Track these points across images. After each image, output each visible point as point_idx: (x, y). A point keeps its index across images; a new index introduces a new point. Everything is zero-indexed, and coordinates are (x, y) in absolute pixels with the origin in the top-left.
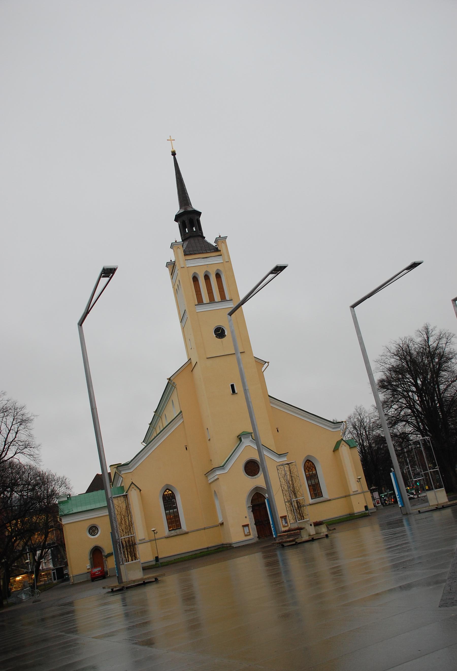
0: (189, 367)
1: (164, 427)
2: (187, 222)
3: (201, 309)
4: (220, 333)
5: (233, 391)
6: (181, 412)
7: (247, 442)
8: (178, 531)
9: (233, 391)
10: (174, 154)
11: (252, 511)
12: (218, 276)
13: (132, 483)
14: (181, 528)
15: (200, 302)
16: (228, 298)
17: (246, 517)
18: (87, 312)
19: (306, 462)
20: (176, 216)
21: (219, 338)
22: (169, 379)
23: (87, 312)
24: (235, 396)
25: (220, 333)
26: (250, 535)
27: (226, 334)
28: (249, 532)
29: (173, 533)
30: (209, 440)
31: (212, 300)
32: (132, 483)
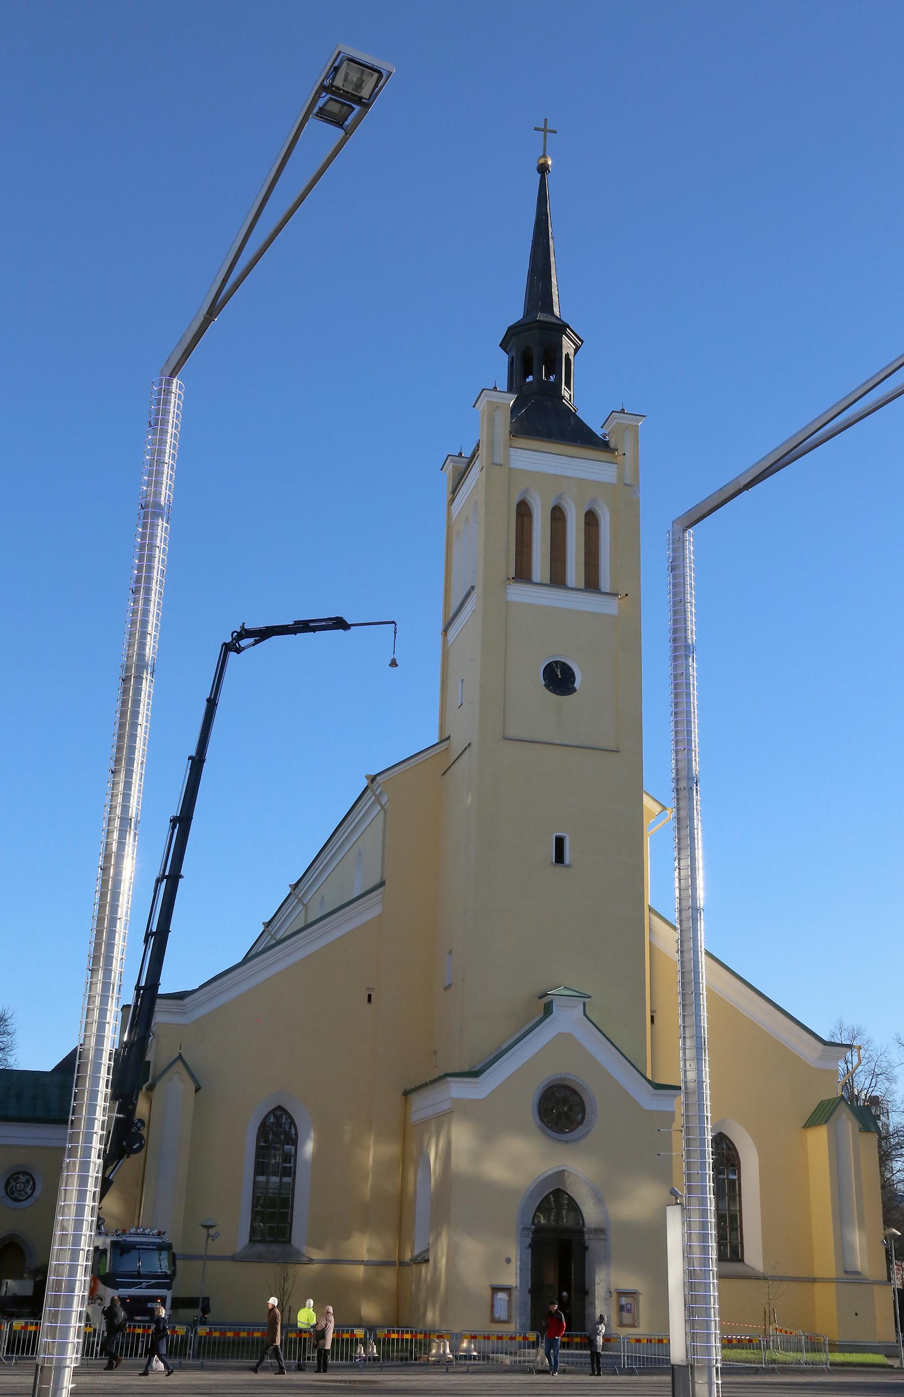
0: (440, 759)
1: (310, 921)
2: (536, 352)
3: (519, 593)
4: (559, 679)
5: (560, 857)
6: (382, 884)
7: (567, 1019)
8: (276, 1248)
9: (560, 857)
10: (543, 169)
11: (531, 1246)
12: (591, 520)
13: (180, 1057)
14: (289, 1241)
15: (523, 574)
16: (605, 583)
17: (508, 1261)
18: (213, 312)
19: (273, 1112)
20: (510, 328)
21: (554, 692)
22: (373, 779)
23: (213, 312)
24: (559, 869)
25: (559, 679)
26: (507, 1322)
27: (577, 685)
28: (510, 1316)
29: (261, 1248)
30: (447, 988)
31: (557, 579)
32: (180, 1057)
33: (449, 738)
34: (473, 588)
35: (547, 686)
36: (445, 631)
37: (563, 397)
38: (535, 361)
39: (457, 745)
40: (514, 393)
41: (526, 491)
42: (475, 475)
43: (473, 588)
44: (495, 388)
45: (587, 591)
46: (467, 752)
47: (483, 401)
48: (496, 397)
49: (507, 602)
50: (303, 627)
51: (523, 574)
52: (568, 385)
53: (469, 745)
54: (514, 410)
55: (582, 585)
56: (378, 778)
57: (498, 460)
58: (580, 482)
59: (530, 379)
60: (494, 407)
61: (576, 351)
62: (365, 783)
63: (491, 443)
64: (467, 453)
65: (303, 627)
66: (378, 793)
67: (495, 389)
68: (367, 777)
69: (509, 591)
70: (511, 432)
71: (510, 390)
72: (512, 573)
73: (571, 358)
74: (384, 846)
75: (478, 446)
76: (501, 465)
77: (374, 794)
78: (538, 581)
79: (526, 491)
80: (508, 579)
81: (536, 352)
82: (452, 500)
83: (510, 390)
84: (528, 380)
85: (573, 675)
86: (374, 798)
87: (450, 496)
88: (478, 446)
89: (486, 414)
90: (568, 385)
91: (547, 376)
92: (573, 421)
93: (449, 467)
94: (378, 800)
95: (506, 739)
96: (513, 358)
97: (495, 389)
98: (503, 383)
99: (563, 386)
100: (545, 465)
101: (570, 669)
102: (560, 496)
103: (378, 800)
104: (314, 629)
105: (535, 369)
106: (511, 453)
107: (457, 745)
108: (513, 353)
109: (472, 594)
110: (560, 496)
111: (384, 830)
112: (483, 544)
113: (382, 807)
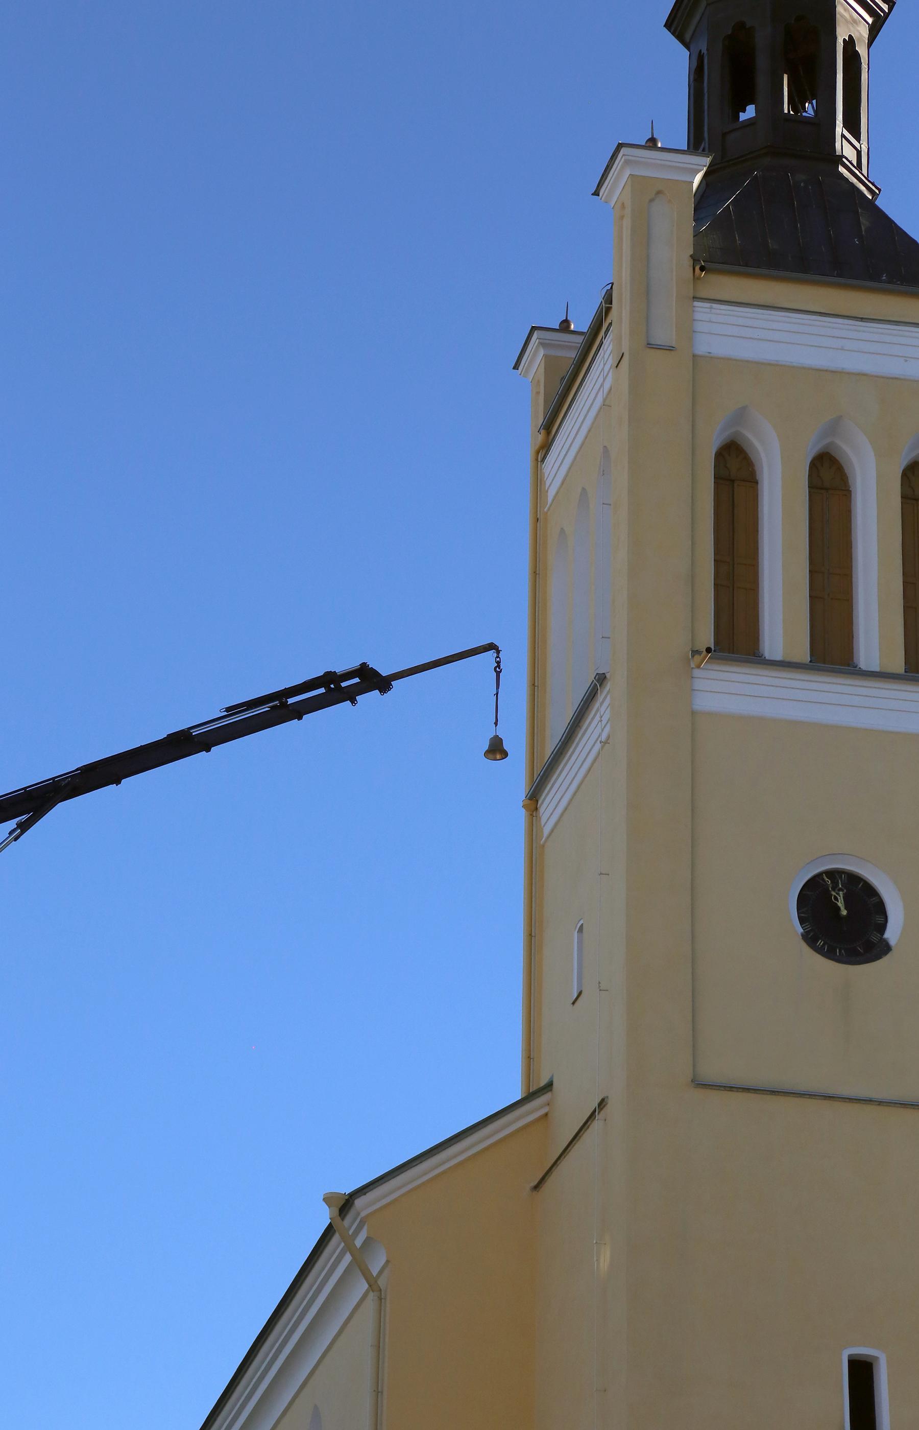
0: (521, 1149)
2: (764, 38)
3: (727, 690)
21: (829, 954)
22: (344, 1205)
23: (498, 674)
27: (892, 934)
33: (549, 1086)
34: (601, 679)
35: (810, 939)
36: (534, 798)
37: (839, 159)
38: (762, 62)
39: (570, 1107)
40: (704, 153)
41: (741, 415)
42: (601, 379)
43: (601, 679)
44: (652, 141)
45: (819, 670)
46: (596, 1125)
47: (618, 186)
48: (656, 167)
49: (693, 713)
50: (278, 708)
51: (735, 637)
52: (853, 125)
53: (602, 1104)
54: (704, 200)
55: (803, 653)
56: (359, 1202)
57: (664, 334)
58: (887, 385)
59: (750, 112)
60: (648, 193)
61: (874, 30)
62: (323, 1217)
63: (645, 291)
64: (581, 323)
65: (278, 708)
66: (359, 1242)
67: (652, 143)
68: (329, 1199)
69: (699, 684)
70: (695, 259)
71: (696, 145)
72: (707, 637)
73: (862, 49)
74: (378, 1393)
75: (608, 298)
76: (671, 349)
77: (349, 1247)
78: (778, 657)
79: (741, 415)
80: (695, 652)
81: (764, 38)
82: (545, 448)
83: (696, 145)
84: (743, 117)
85: (880, 908)
86: (348, 1258)
87: (540, 438)
88: (608, 298)
89: (628, 211)
90: (853, 125)
91: (797, 102)
92: (865, 223)
93: (536, 358)
94: (359, 1265)
95: (700, 1084)
96: (701, 57)
97: (652, 143)
98: (675, 127)
99: (839, 128)
100: (789, 340)
101: (870, 891)
102: (834, 426)
103: (359, 1265)
104: (298, 712)
105: (762, 82)
106: (698, 316)
107: (570, 1107)
108: (703, 45)
109: (600, 697)
110: (834, 426)
111: (378, 1347)
112: (632, 562)
113: (373, 1285)
